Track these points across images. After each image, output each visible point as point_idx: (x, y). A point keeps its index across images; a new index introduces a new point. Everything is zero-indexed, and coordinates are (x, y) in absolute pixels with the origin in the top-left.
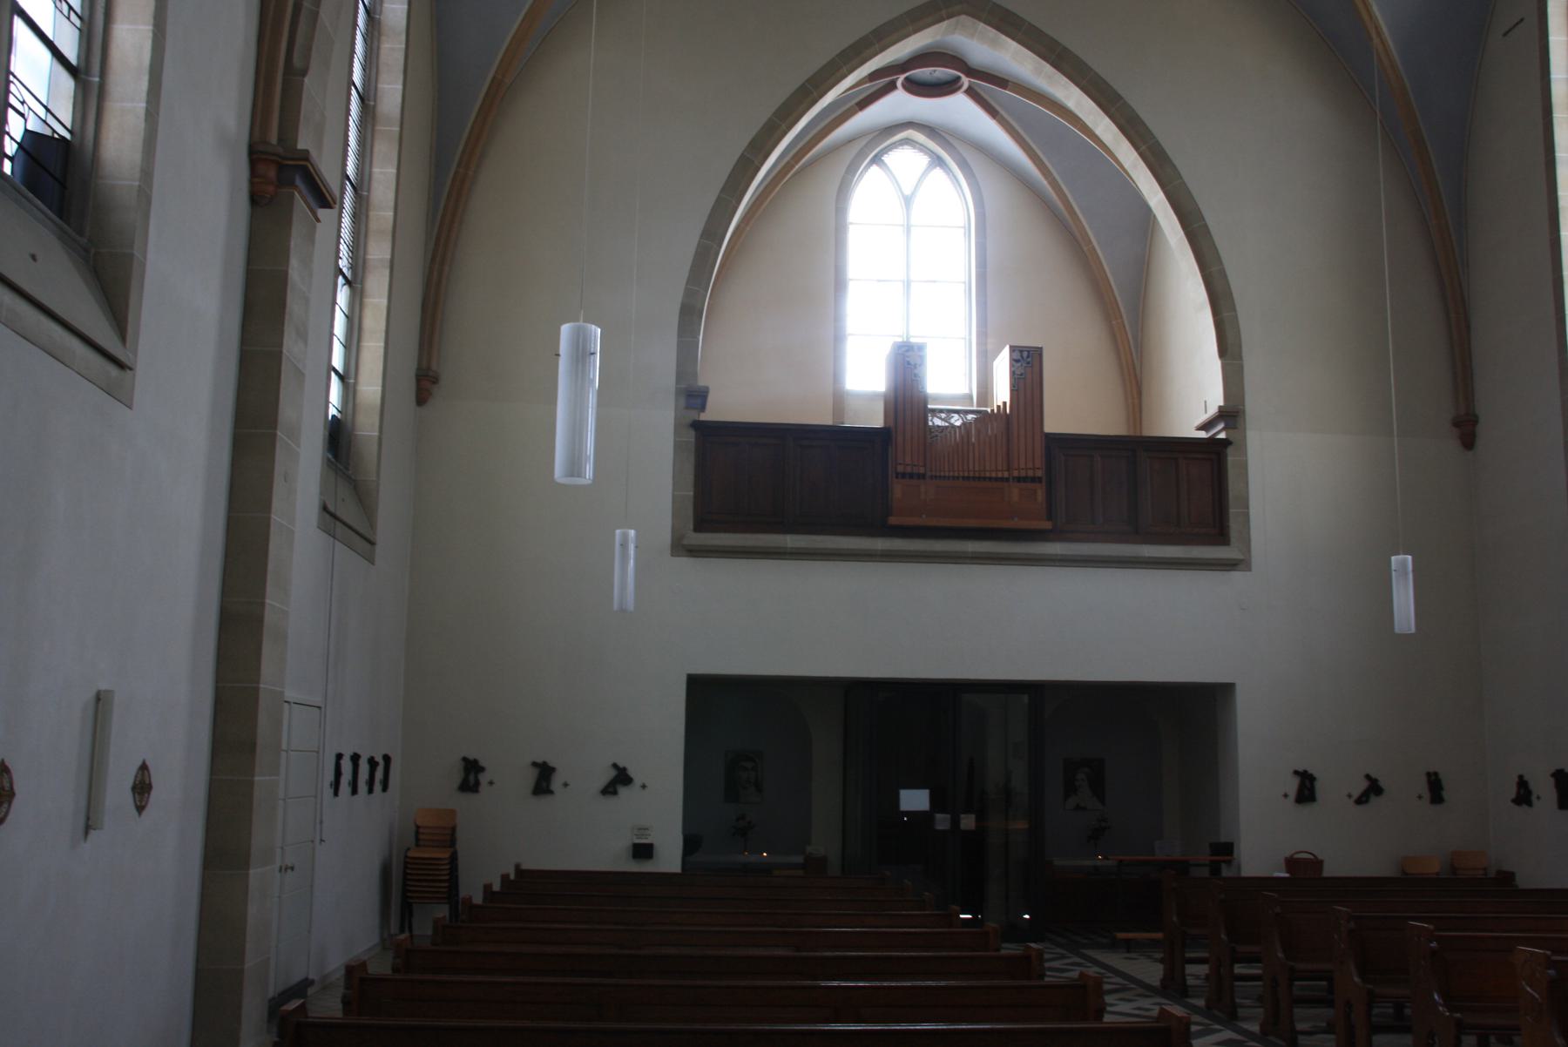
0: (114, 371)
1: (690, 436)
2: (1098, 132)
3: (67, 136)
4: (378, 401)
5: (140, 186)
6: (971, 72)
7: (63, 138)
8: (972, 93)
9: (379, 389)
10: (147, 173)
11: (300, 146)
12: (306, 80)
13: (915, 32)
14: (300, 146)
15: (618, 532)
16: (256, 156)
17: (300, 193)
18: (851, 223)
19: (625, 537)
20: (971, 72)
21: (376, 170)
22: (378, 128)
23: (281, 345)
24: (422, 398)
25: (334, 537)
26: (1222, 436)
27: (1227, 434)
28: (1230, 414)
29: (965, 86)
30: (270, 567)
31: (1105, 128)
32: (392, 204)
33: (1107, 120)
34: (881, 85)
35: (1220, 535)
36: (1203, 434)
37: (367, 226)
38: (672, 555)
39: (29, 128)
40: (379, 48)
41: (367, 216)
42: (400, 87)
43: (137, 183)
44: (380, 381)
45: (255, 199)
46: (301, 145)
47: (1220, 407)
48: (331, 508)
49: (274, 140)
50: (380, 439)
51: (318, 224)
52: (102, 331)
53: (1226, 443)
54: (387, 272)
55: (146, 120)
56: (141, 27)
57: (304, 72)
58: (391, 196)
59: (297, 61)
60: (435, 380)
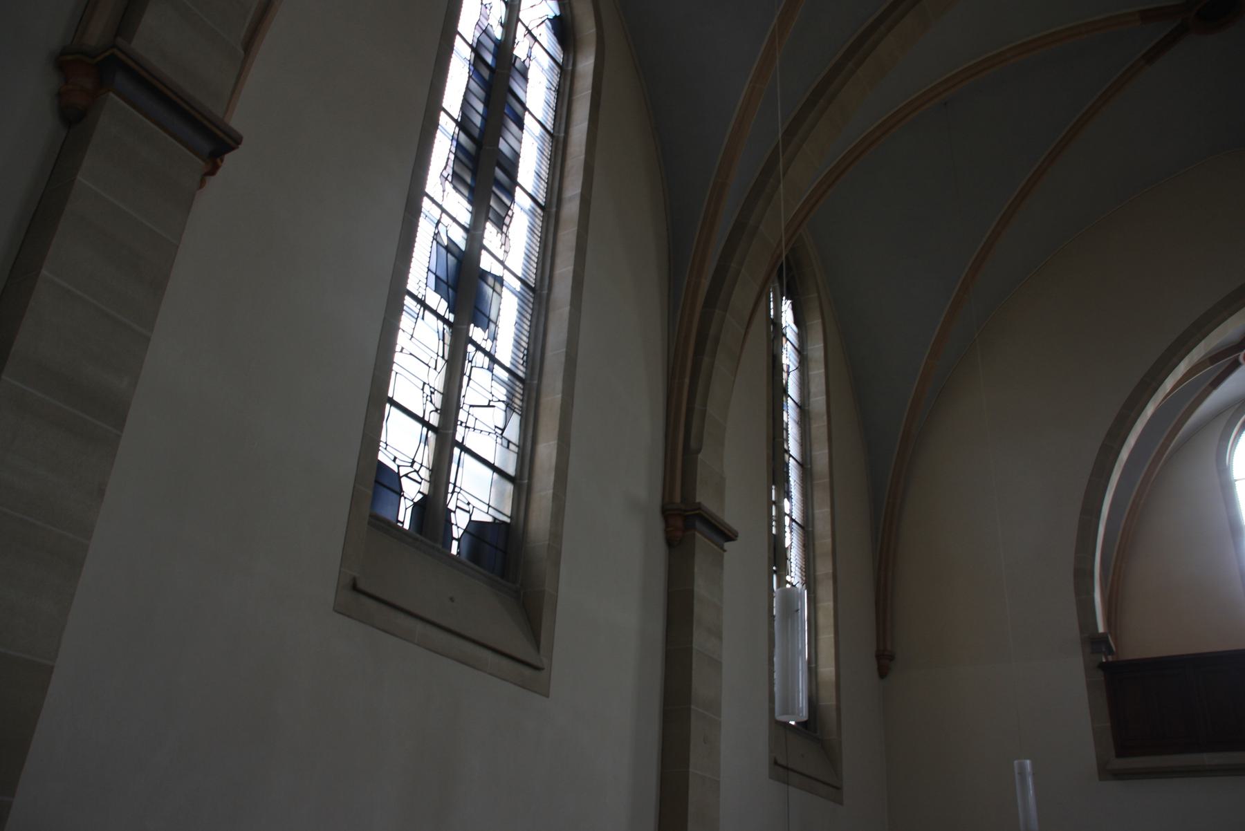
0: (528, 672)
1: (1100, 676)
3: (508, 520)
4: (833, 678)
5: (549, 544)
7: (504, 522)
9: (833, 669)
10: (556, 534)
11: (697, 501)
12: (700, 456)
13: (1231, 315)
14: (697, 501)
15: (1016, 762)
16: (667, 513)
17: (701, 533)
18: (1236, 480)
19: (1022, 767)
21: (817, 512)
22: (815, 482)
23: (691, 642)
24: (883, 672)
25: (788, 784)
30: (692, 809)
32: (829, 533)
34: (1227, 365)
37: (814, 552)
38: (1100, 780)
39: (472, 519)
40: (810, 429)
41: (814, 544)
42: (826, 451)
43: (547, 542)
44: (833, 663)
45: (670, 542)
46: (698, 500)
48: (782, 761)
49: (678, 499)
50: (838, 709)
51: (725, 554)
52: (518, 644)
54: (831, 582)
55: (553, 501)
56: (551, 443)
57: (699, 451)
58: (828, 527)
59: (693, 444)
60: (892, 658)
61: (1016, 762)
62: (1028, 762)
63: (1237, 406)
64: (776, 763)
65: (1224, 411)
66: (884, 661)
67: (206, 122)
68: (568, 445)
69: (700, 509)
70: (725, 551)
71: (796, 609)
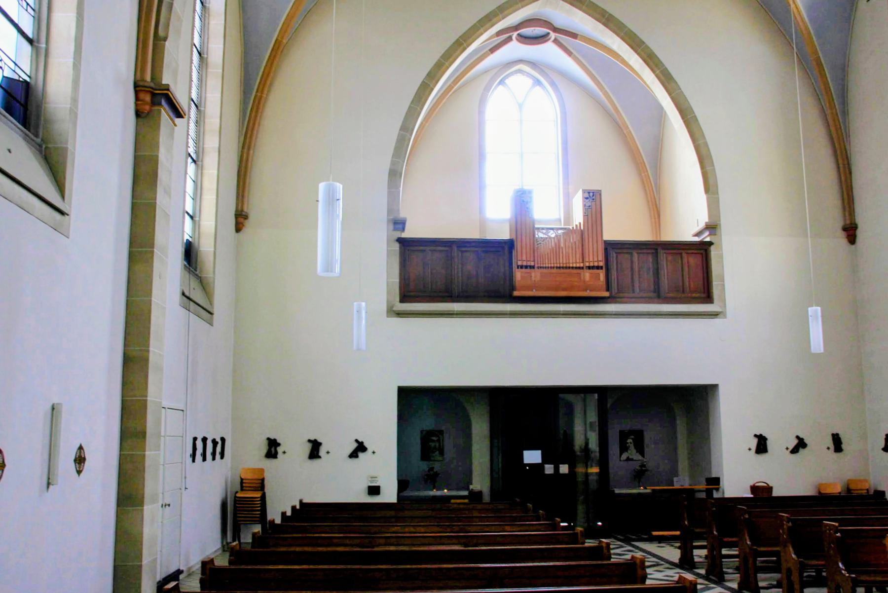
2: (631, 63)
5: (70, 108)
6: (556, 30)
8: (556, 41)
9: (213, 223)
12: (167, 43)
16: (138, 88)
17: (165, 109)
20: (556, 30)
22: (209, 70)
23: (155, 199)
24: (238, 229)
26: (708, 239)
27: (710, 238)
28: (712, 227)
29: (553, 38)
31: (635, 61)
33: (636, 56)
35: (708, 298)
36: (697, 239)
38: (387, 317)
39: (5, 75)
42: (222, 46)
47: (706, 223)
48: (187, 294)
49: (148, 78)
51: (176, 128)
53: (710, 244)
59: (161, 33)
60: (246, 217)
61: (355, 303)
62: (364, 304)
63: (501, 67)
64: (183, 294)
65: (491, 70)
66: (241, 219)
67: (843, 178)
68: (83, 19)
69: (168, 90)
70: (175, 125)
71: (338, 198)
